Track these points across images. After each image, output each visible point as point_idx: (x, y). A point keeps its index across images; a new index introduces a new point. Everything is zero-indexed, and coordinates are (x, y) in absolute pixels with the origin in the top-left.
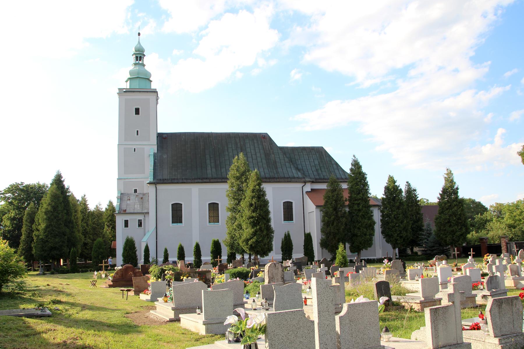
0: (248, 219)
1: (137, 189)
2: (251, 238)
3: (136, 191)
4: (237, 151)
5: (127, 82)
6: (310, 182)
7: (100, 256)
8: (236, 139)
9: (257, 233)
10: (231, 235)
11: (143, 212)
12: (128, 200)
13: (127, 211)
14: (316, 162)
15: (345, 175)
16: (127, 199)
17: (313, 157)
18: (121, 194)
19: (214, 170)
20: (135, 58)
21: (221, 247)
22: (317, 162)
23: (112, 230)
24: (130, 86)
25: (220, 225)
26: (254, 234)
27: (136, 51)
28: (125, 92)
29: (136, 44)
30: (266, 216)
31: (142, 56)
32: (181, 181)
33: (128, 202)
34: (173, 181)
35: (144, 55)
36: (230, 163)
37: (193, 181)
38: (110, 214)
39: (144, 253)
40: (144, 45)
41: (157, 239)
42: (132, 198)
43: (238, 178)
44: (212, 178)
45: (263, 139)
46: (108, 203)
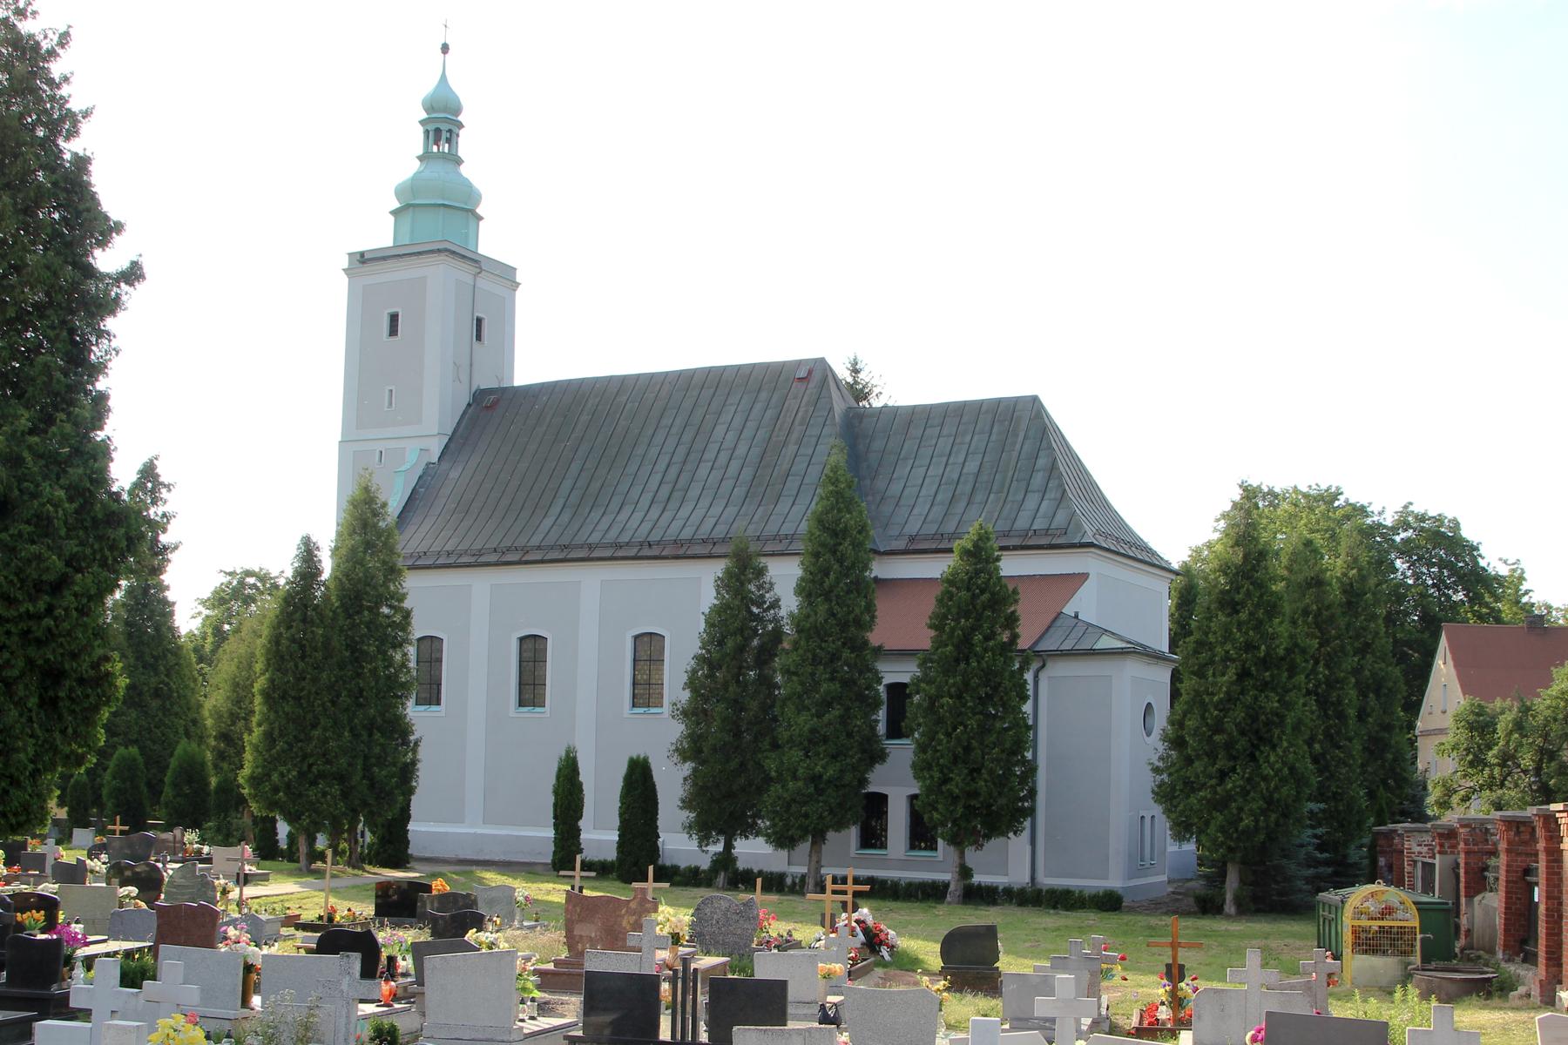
25: (941, 858)
29: (428, 86)
35: (460, 126)
40: (461, 88)
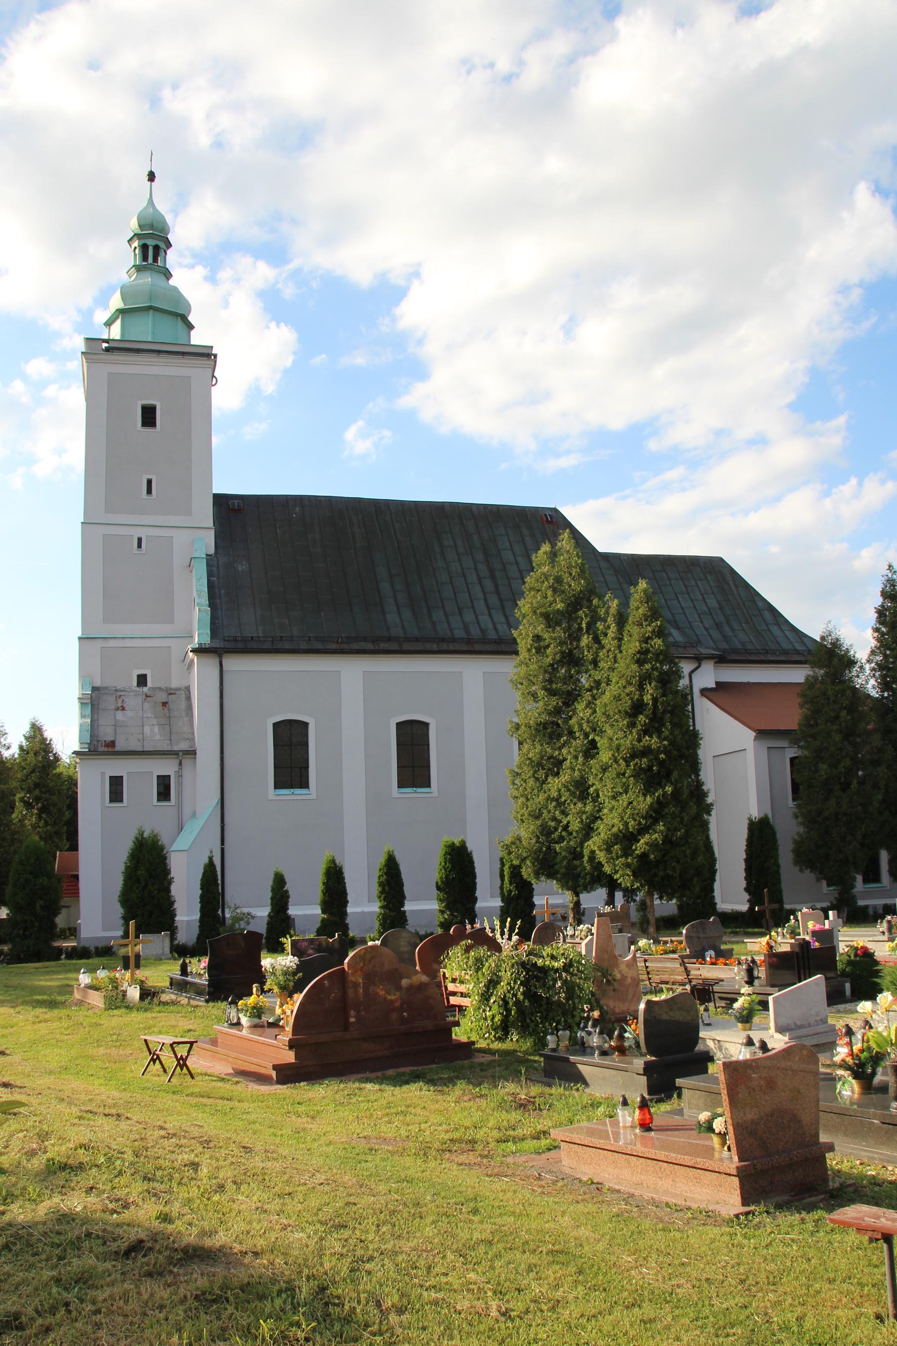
0: (624, 759)
1: (146, 675)
2: (643, 830)
3: (142, 680)
4: (473, 557)
5: (113, 327)
6: (709, 657)
7: (39, 904)
8: (464, 521)
9: (666, 810)
10: (539, 822)
11: (175, 748)
12: (117, 709)
13: (116, 745)
14: (713, 603)
15: (803, 643)
16: (113, 707)
17: (698, 586)
18: (94, 689)
19: (407, 614)
20: (137, 251)
21: (473, 868)
22: (715, 601)
23: (39, 817)
24: (123, 334)
26: (656, 814)
27: (141, 226)
28: (107, 350)
30: (688, 748)
31: (162, 245)
32: (304, 645)
33: (120, 715)
34: (279, 645)
36: (467, 585)
37: (345, 646)
38: (35, 765)
39: (202, 889)
41: (223, 843)
42: (132, 702)
43: (550, 620)
44: (407, 640)
45: (547, 526)
46: (26, 729)
